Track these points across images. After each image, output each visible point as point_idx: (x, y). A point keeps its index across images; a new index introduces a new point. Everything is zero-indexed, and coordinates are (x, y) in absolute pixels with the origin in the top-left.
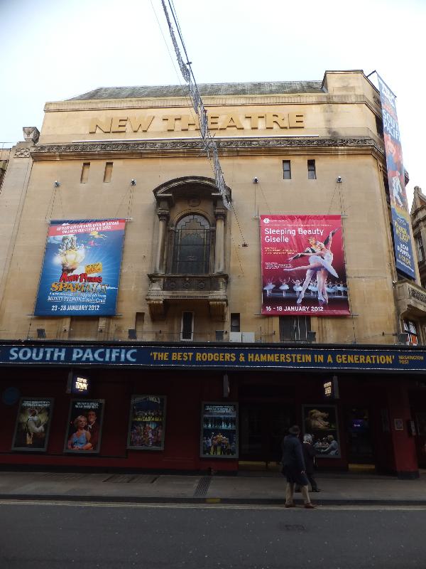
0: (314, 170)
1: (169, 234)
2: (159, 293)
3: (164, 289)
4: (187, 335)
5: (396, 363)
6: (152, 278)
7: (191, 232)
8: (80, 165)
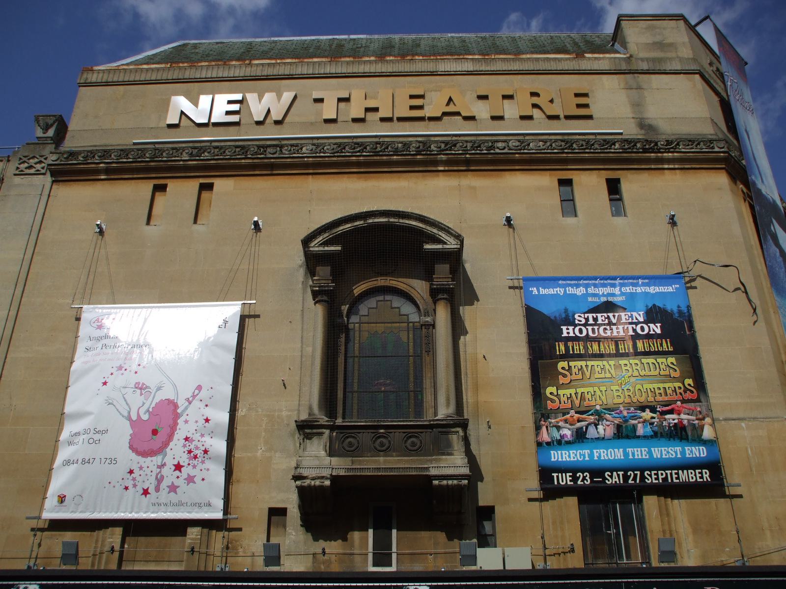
0: (621, 199)
1: (336, 331)
2: (319, 462)
3: (331, 453)
4: (382, 558)
5: (71, 555)
6: (306, 429)
7: (380, 328)
8: (146, 188)
